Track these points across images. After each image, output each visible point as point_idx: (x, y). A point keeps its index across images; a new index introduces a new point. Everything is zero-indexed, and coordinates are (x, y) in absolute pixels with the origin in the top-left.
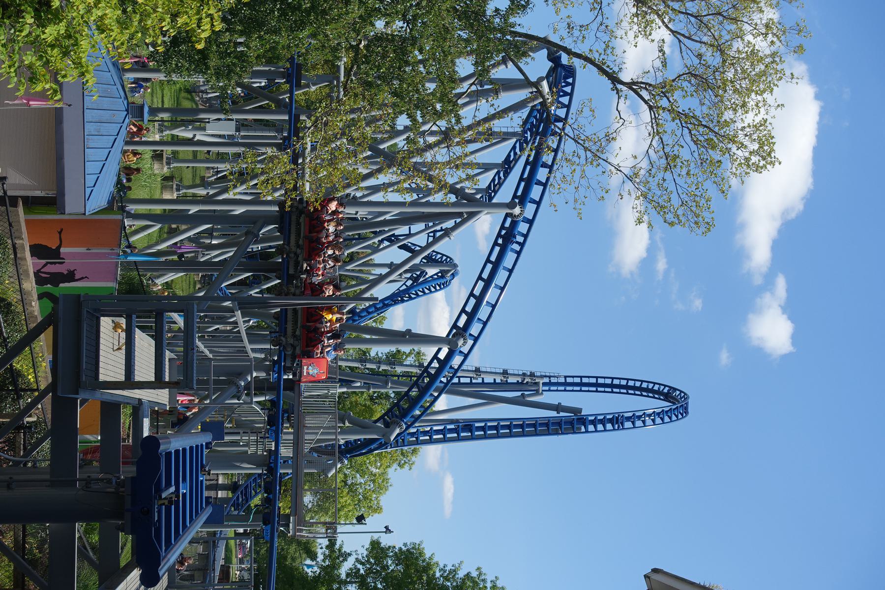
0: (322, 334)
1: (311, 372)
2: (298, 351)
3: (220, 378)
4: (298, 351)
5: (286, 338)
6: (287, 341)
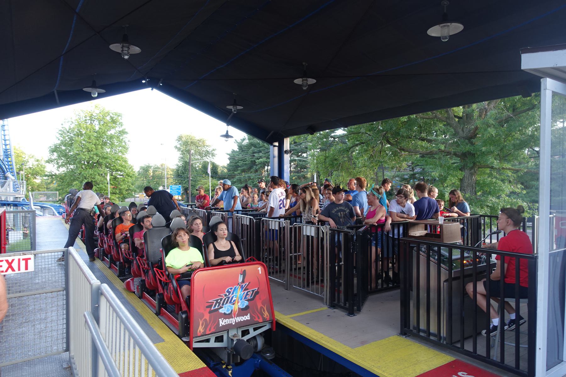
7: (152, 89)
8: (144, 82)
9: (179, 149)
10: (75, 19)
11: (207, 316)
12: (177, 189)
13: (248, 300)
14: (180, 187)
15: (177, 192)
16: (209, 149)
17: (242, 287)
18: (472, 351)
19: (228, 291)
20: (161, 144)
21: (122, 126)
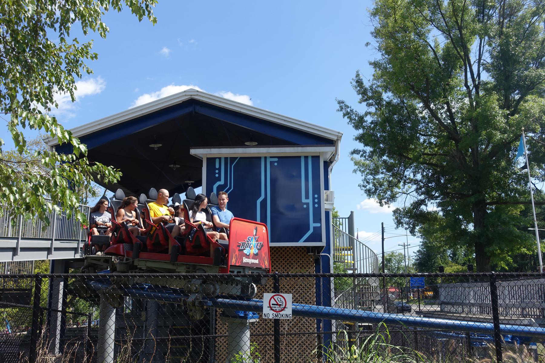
0: (189, 227)
1: (254, 251)
2: (213, 272)
3: (367, 324)
4: (213, 272)
5: (190, 292)
6: (196, 292)
8: (381, 145)
10: (507, 268)
11: (237, 253)
13: (258, 249)
18: (185, 193)
19: (248, 239)
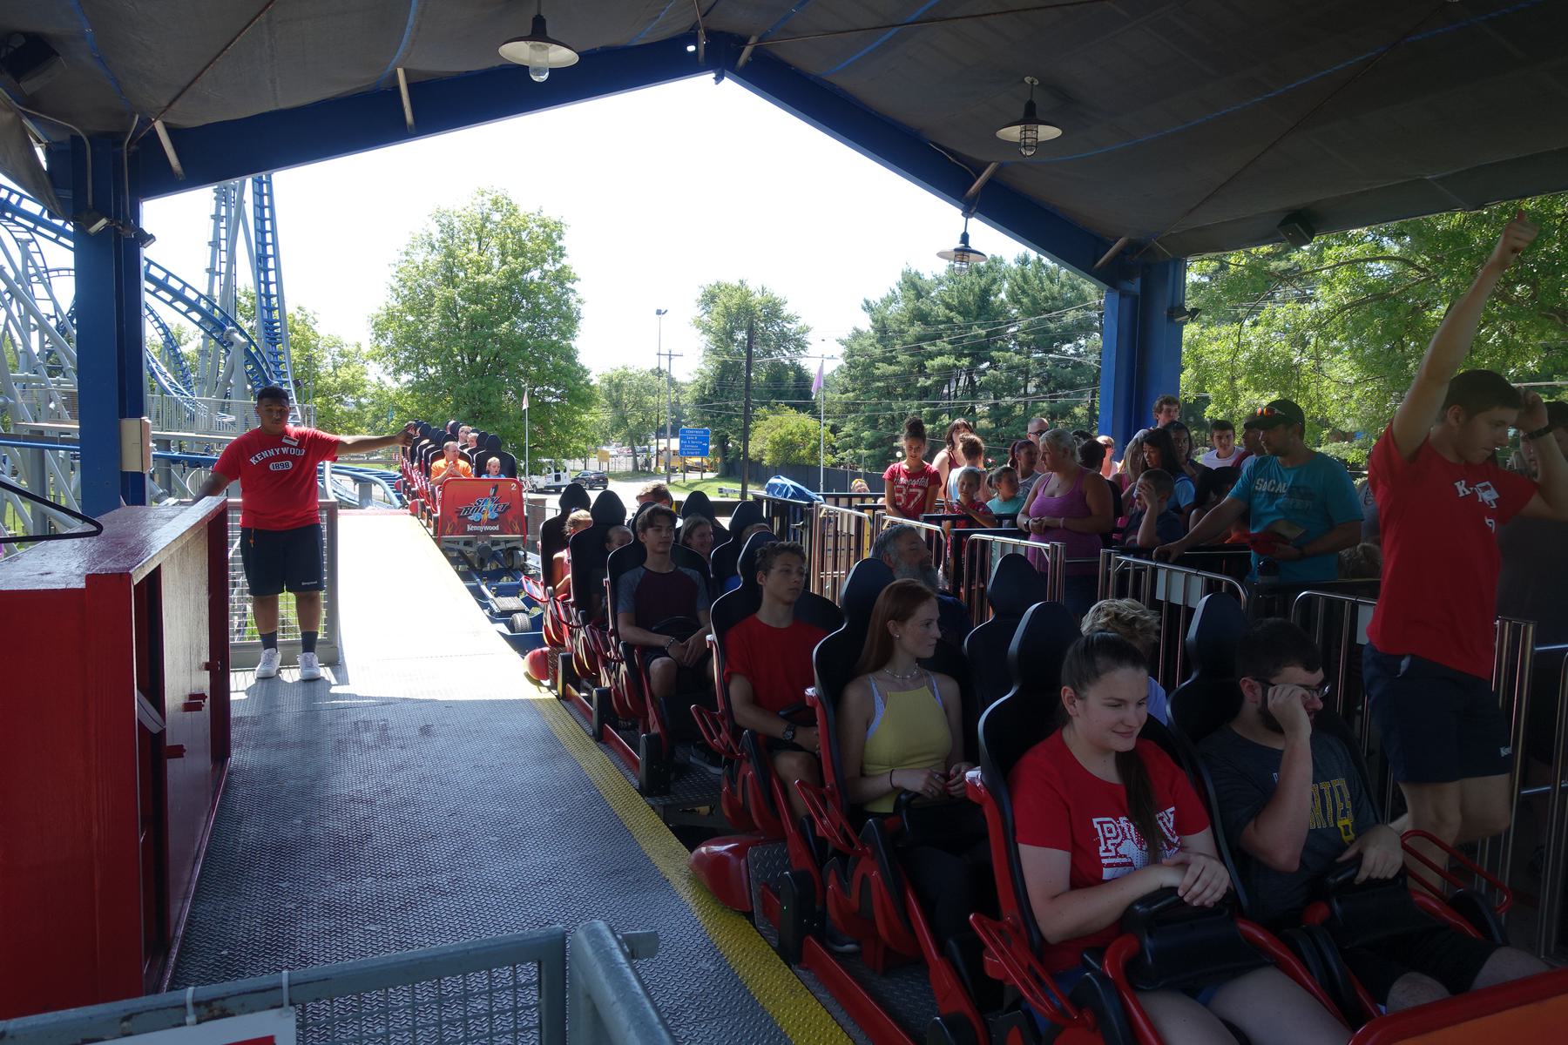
7: (718, 79)
9: (707, 330)
12: (699, 439)
14: (706, 432)
15: (700, 446)
16: (791, 327)
17: (493, 500)
20: (659, 312)
21: (562, 255)
